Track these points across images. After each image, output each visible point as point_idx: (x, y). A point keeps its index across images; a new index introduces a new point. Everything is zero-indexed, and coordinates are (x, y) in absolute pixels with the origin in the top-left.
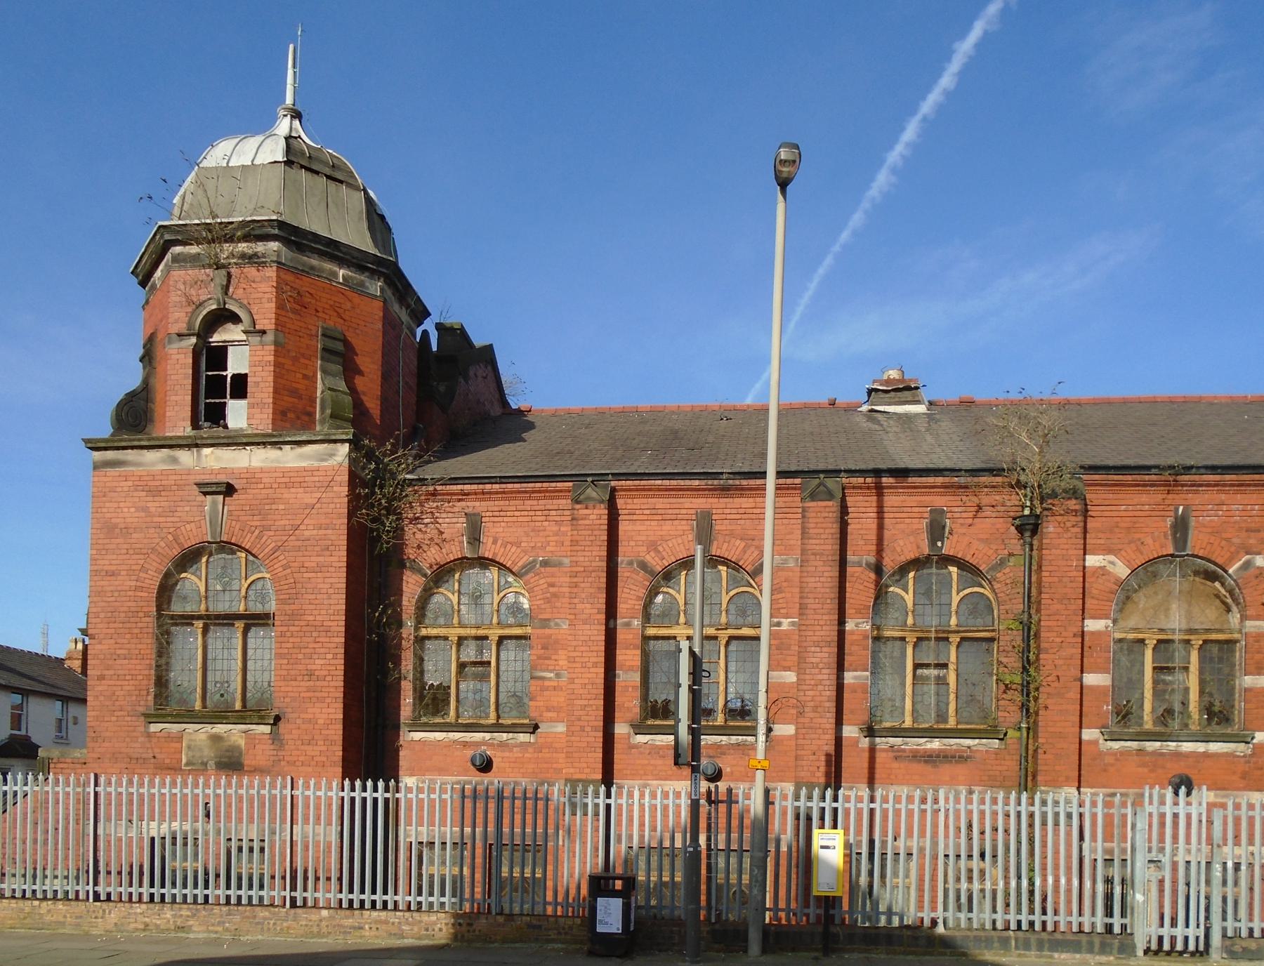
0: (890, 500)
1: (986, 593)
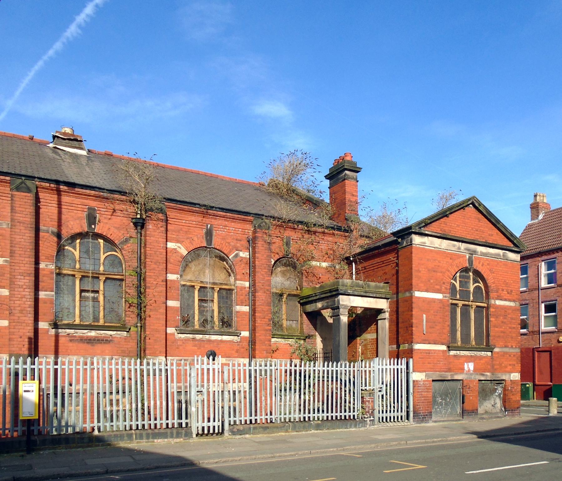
0: (65, 199)
1: (118, 255)
